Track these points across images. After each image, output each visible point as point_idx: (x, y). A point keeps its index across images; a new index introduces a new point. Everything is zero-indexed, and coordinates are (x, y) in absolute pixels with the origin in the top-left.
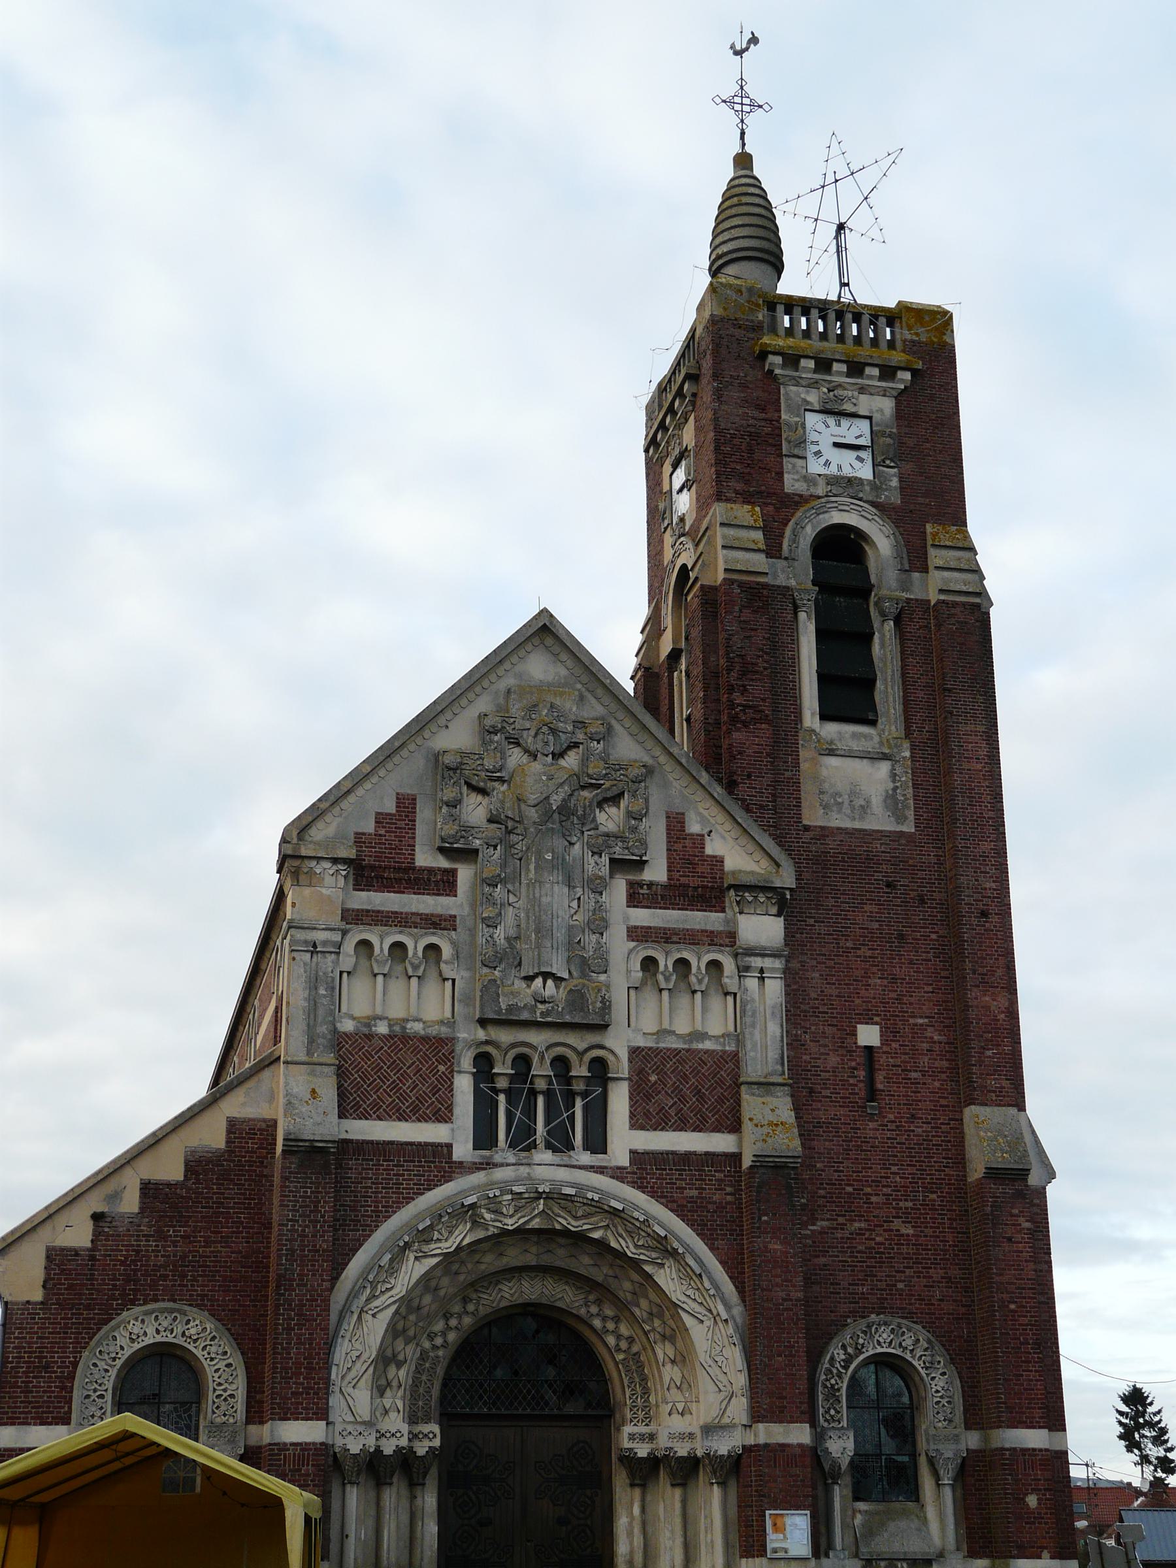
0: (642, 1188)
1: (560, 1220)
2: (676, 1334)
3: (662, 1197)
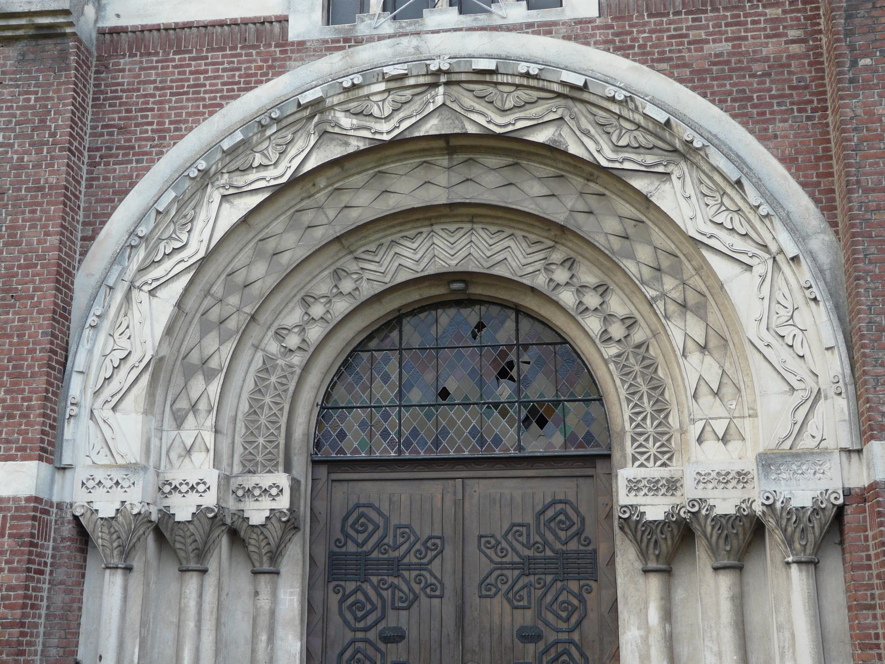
0: (623, 50)
1: (474, 117)
2: (704, 300)
3: (660, 61)
